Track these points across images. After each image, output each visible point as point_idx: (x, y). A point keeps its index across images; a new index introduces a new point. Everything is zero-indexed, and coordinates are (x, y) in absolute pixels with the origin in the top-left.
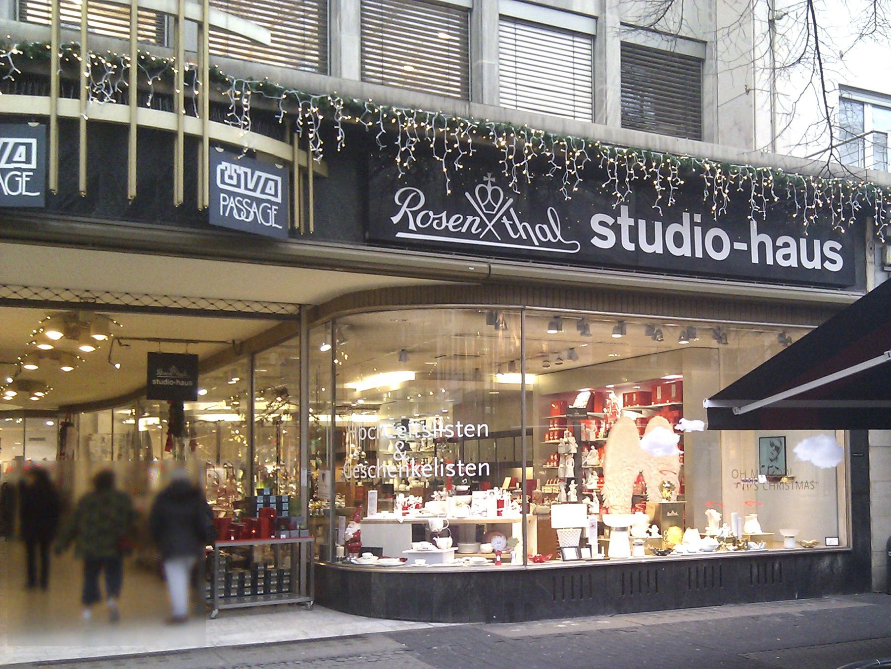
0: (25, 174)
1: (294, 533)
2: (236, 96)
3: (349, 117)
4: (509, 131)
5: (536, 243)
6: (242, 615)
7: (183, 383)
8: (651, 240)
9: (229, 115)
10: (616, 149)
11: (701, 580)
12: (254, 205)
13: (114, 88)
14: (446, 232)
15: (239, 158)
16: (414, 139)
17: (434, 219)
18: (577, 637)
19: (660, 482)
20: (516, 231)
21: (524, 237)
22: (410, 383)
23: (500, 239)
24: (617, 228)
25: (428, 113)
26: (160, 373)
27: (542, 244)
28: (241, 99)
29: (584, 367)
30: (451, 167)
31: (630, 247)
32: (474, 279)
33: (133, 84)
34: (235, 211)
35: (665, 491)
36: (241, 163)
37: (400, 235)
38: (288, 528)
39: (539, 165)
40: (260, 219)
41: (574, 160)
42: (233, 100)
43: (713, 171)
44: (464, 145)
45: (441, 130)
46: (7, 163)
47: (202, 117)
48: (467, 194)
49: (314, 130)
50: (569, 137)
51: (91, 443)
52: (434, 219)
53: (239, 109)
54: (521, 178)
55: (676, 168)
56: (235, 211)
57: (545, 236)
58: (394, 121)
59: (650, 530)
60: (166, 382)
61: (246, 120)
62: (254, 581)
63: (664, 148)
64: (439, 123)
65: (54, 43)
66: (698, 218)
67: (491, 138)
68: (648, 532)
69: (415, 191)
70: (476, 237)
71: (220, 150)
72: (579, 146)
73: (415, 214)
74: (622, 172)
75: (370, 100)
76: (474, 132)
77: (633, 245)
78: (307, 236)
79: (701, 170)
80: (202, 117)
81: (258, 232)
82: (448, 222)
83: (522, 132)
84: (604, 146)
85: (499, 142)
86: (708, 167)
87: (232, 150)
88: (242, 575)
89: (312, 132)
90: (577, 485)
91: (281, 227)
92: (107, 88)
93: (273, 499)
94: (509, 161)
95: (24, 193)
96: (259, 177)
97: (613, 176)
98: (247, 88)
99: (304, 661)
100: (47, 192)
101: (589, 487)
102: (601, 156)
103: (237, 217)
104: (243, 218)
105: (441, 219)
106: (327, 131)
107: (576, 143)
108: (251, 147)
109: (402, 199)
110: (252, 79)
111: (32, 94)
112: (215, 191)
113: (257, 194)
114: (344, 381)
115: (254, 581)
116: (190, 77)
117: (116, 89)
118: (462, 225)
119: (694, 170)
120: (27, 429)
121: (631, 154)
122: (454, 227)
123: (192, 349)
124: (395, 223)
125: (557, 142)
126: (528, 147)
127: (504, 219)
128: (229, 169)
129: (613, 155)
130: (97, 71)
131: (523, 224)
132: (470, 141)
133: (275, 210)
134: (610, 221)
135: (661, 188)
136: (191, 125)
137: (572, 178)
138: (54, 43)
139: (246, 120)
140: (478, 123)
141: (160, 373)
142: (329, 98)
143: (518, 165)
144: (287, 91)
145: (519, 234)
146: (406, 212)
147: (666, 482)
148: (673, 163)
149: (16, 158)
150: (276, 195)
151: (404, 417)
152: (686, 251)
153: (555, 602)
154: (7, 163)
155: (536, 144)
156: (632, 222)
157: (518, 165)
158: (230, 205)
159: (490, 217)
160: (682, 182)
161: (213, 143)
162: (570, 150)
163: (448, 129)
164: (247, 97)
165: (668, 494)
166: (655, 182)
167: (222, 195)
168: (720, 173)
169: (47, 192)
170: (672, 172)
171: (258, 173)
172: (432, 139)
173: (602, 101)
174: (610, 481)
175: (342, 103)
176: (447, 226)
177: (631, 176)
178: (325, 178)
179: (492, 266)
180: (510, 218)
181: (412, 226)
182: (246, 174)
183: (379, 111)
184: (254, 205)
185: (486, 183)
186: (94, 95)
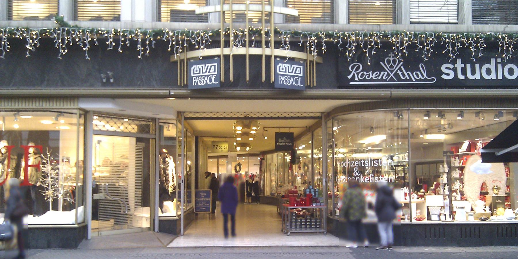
0: (214, 76)
1: (318, 204)
2: (284, 38)
3: (328, 39)
4: (397, 34)
5: (414, 80)
6: (299, 235)
7: (288, 144)
8: (473, 73)
9: (281, 45)
10: (451, 34)
11: (505, 233)
12: (292, 78)
13: (241, 41)
14: (371, 80)
15: (286, 61)
16: (354, 44)
17: (366, 75)
18: (429, 254)
19: (493, 186)
20: (404, 75)
21: (408, 78)
22: (383, 141)
23: (396, 80)
24: (455, 70)
25: (360, 32)
26: (280, 140)
27: (416, 80)
28: (286, 39)
29: (467, 130)
30: (370, 53)
31: (461, 77)
32: (385, 98)
33: (247, 40)
34: (284, 82)
35: (495, 190)
36: (286, 63)
37: (351, 83)
38: (316, 202)
39: (412, 47)
40: (294, 83)
41: (429, 43)
42: (283, 39)
43: (503, 38)
44: (376, 43)
45: (366, 38)
46: (209, 73)
47: (271, 48)
48: (381, 63)
49: (313, 46)
50: (427, 32)
51: (271, 167)
52: (366, 75)
53: (285, 42)
54: (403, 54)
55: (482, 39)
56: (284, 82)
57: (418, 76)
58: (346, 38)
59: (485, 209)
60: (282, 144)
61: (288, 46)
62: (306, 222)
63: (476, 30)
64: (365, 35)
65: (222, 28)
66: (499, 60)
67: (389, 38)
68: (484, 210)
69: (357, 64)
70: (385, 80)
71: (278, 59)
72: (431, 36)
73: (358, 74)
74: (453, 45)
75: (336, 31)
76: (381, 37)
77: (464, 76)
78: (314, 87)
79: (497, 38)
80: (271, 48)
81: (294, 88)
82: (372, 75)
83: (403, 34)
84: (444, 34)
85: (392, 40)
86: (500, 37)
87: (283, 59)
88: (301, 220)
89: (313, 47)
90: (449, 187)
91: (302, 86)
92: (239, 42)
93: (313, 190)
94: (397, 48)
95: (214, 83)
96: (294, 67)
97: (448, 46)
98: (288, 34)
99: (310, 253)
100: (221, 82)
101: (455, 188)
102: (442, 39)
103: (285, 84)
104: (287, 84)
105: (369, 75)
106: (319, 46)
107: (430, 35)
108: (290, 56)
109: (352, 68)
110: (290, 30)
111: (216, 48)
112: (276, 75)
113: (293, 74)
114: (357, 140)
115: (306, 222)
116: (267, 34)
117: (242, 42)
118: (379, 76)
119: (493, 39)
120: (250, 161)
121: (458, 36)
122: (375, 77)
123: (291, 131)
124: (349, 78)
125: (420, 36)
126: (406, 40)
127: (399, 72)
128: (282, 66)
129: (449, 38)
130: (236, 36)
131: (407, 72)
132: (379, 41)
133: (300, 79)
134: (451, 66)
135: (474, 50)
136: (268, 52)
137: (428, 51)
138: (222, 28)
139: (288, 46)
140: (383, 33)
141: (280, 140)
142: (319, 33)
143: (401, 48)
144: (303, 33)
145: (405, 77)
146: (354, 74)
147: (496, 186)
148: (481, 37)
149: (211, 71)
150: (300, 73)
151: (392, 155)
152: (493, 76)
153: (426, 239)
154: (209, 73)
155: (410, 38)
156: (463, 66)
157: (401, 48)
158: (282, 79)
159: (392, 71)
160: (485, 46)
161: (276, 57)
162: (427, 38)
163: (369, 37)
164: (288, 37)
165: (496, 192)
166: (471, 47)
167: (279, 76)
168: (507, 39)
169: (221, 82)
170: (480, 42)
171: (293, 66)
172: (362, 43)
173: (462, 8)
174: (467, 185)
175: (325, 34)
176: (372, 77)
177: (458, 46)
178: (322, 63)
179: (392, 92)
180: (401, 70)
181: (357, 79)
182: (288, 67)
183: (339, 35)
184: (292, 78)
185: (390, 57)
186: (235, 45)
